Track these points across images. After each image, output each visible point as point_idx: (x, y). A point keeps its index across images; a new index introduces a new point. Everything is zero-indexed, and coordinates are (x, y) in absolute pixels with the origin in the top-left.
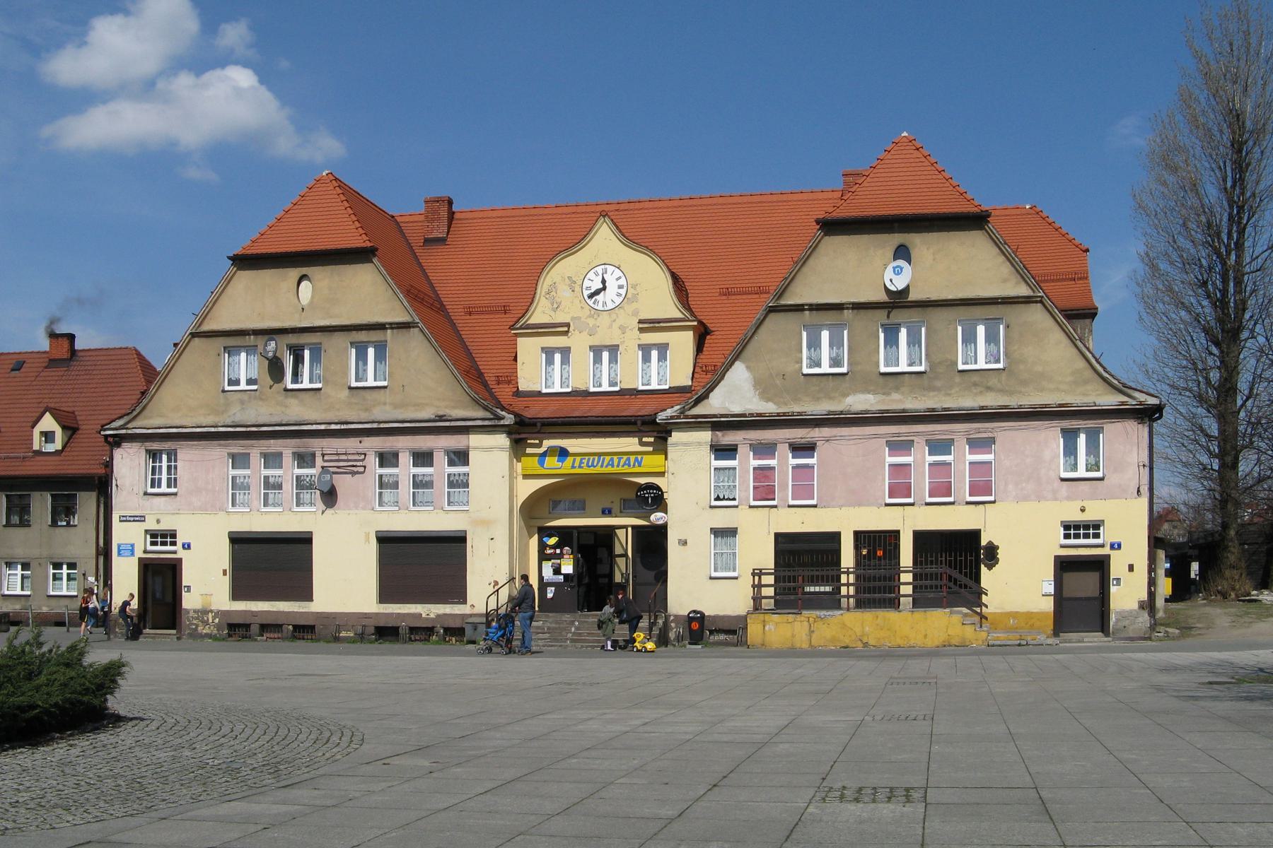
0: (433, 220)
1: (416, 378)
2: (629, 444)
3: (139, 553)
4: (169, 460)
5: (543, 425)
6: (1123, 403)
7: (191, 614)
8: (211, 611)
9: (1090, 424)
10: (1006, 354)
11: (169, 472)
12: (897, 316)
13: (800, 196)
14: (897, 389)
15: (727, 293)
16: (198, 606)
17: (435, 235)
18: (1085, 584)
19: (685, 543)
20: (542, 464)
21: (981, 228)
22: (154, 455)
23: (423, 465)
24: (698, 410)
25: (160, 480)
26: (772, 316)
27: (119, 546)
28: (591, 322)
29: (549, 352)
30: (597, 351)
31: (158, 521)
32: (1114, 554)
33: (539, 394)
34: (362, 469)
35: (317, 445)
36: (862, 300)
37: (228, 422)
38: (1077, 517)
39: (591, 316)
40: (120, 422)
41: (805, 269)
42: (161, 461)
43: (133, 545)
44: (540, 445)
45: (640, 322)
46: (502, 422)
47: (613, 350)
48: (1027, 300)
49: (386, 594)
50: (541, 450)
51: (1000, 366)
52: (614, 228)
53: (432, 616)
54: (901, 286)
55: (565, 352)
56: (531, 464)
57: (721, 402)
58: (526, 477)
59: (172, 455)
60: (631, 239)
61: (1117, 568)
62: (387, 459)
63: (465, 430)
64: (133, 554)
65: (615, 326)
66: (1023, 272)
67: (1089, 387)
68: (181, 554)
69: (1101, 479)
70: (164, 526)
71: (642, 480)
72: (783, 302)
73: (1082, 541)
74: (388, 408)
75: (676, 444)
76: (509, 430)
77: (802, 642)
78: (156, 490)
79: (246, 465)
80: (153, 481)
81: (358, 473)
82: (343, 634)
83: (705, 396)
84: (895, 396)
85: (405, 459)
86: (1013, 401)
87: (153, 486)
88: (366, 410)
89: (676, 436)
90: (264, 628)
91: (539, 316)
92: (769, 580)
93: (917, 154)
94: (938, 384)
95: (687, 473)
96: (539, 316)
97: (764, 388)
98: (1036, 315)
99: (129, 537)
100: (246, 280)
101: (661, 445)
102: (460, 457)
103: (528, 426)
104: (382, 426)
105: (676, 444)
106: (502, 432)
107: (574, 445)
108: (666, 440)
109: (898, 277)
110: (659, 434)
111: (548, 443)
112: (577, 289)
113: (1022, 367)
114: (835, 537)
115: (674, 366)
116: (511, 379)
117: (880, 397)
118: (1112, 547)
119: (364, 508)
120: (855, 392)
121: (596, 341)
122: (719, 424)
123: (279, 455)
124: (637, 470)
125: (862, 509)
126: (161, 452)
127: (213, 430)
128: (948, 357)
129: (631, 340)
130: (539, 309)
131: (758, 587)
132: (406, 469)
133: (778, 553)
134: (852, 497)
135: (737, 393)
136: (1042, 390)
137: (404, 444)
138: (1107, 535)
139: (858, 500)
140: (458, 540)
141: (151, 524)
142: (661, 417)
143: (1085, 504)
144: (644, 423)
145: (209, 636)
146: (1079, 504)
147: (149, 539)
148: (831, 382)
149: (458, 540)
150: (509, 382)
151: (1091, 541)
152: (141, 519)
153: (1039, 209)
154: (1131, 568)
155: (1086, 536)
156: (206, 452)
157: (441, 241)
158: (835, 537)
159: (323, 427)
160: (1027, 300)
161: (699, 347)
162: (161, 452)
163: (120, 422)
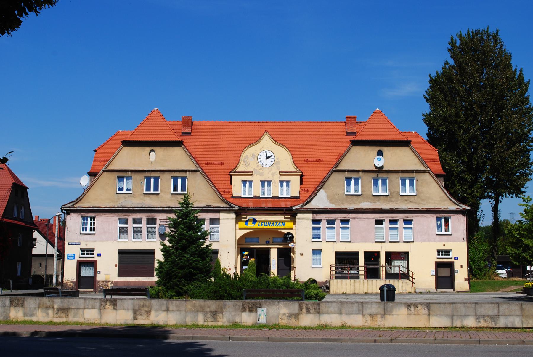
0: (185, 125)
2: (281, 218)
3: (77, 258)
4: (91, 220)
6: (457, 209)
7: (101, 282)
9: (446, 215)
10: (417, 190)
11: (91, 225)
12: (381, 175)
13: (329, 124)
14: (378, 201)
15: (307, 161)
16: (104, 280)
17: (186, 131)
18: (445, 272)
22: (84, 218)
24: (307, 206)
25: (86, 228)
26: (334, 173)
27: (68, 255)
28: (261, 171)
29: (244, 182)
30: (263, 182)
31: (86, 245)
32: (456, 261)
33: (241, 197)
35: (157, 216)
37: (119, 205)
38: (442, 248)
40: (71, 204)
41: (345, 157)
42: (87, 220)
43: (74, 255)
44: (246, 218)
45: (280, 172)
46: (234, 209)
47: (269, 182)
48: (424, 172)
50: (246, 220)
51: (415, 194)
52: (270, 137)
54: (380, 165)
55: (251, 182)
56: (242, 225)
57: (315, 204)
58: (240, 229)
60: (276, 141)
61: (457, 266)
63: (218, 212)
64: (74, 258)
65: (270, 173)
67: (446, 202)
68: (96, 258)
69: (451, 235)
70: (89, 247)
71: (286, 231)
72: (338, 169)
73: (444, 256)
75: (299, 219)
76: (236, 212)
78: (85, 232)
80: (83, 228)
83: (310, 201)
84: (378, 203)
86: (420, 207)
87: (83, 230)
89: (299, 216)
91: (240, 168)
92: (334, 268)
93: (382, 117)
94: (393, 199)
95: (302, 228)
96: (240, 168)
97: (331, 199)
98: (427, 176)
99: (72, 252)
100: (127, 151)
101: (293, 219)
105: (299, 219)
107: (258, 218)
108: (295, 217)
109: (379, 162)
110: (291, 214)
111: (249, 217)
112: (256, 159)
113: (422, 195)
114: (357, 253)
115: (294, 189)
116: (229, 191)
117: (373, 204)
118: (455, 258)
120: (364, 201)
121: (263, 178)
124: (283, 227)
126: (87, 217)
127: (113, 209)
128: (397, 190)
129: (277, 178)
130: (241, 166)
131: (331, 271)
133: (337, 259)
134: (363, 238)
135: (321, 201)
136: (429, 203)
138: (453, 255)
141: (83, 246)
142: (294, 208)
144: (286, 210)
146: (443, 243)
147: (81, 252)
148: (355, 198)
150: (228, 192)
151: (447, 256)
152: (79, 244)
153: (418, 133)
154: (462, 266)
155: (445, 255)
156: (109, 217)
157: (189, 133)
158: (357, 253)
159: (161, 209)
160: (424, 172)
161: (301, 183)
162: (87, 217)
163: (71, 204)
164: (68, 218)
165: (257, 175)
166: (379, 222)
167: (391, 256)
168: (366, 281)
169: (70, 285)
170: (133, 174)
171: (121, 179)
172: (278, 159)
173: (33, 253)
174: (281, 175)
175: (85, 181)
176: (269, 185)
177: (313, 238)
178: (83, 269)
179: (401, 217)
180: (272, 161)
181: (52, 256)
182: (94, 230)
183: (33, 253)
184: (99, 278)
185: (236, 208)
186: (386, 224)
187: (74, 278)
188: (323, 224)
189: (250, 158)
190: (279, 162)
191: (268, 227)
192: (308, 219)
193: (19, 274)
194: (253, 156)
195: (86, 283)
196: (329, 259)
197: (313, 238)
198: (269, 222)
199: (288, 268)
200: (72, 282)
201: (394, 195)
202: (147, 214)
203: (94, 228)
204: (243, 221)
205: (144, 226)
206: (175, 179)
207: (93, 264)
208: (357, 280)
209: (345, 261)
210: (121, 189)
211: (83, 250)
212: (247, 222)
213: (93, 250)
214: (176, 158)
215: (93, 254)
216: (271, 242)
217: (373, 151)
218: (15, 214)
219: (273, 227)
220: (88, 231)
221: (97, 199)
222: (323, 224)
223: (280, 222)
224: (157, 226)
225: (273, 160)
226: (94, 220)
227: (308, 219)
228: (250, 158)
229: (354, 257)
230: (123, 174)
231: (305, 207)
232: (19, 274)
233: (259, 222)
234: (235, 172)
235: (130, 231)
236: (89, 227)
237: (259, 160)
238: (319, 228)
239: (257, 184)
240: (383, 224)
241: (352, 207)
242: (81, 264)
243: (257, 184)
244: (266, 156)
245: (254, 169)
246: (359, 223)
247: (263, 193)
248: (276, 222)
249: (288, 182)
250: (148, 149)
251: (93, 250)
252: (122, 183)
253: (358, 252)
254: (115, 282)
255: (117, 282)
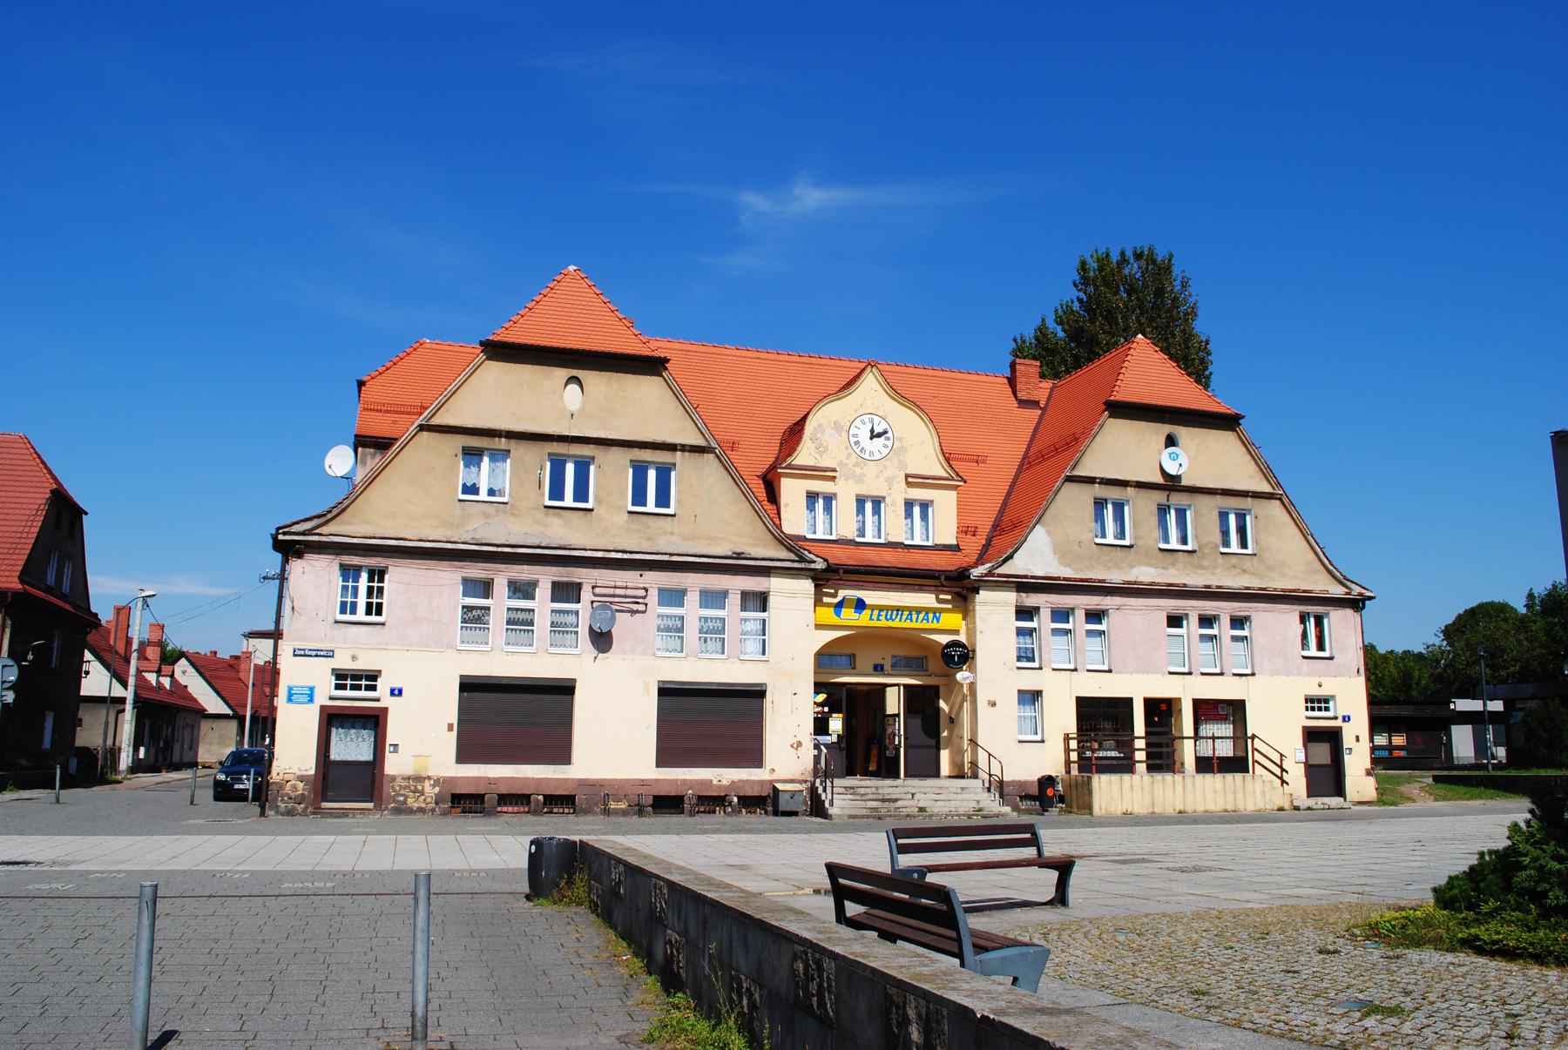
1: (706, 510)
2: (927, 599)
3: (322, 699)
4: (371, 579)
5: (846, 572)
7: (399, 782)
8: (429, 778)
10: (1196, 536)
14: (1173, 564)
16: (410, 772)
19: (994, 704)
20: (838, 614)
21: (1233, 430)
22: (349, 572)
23: (669, 605)
24: (1002, 570)
25: (354, 605)
27: (290, 689)
28: (858, 471)
29: (812, 497)
30: (861, 501)
31: (354, 658)
34: (641, 608)
36: (1142, 480)
37: (467, 537)
38: (1316, 692)
39: (857, 465)
40: (308, 525)
42: (356, 579)
43: (312, 689)
44: (834, 595)
45: (907, 476)
47: (877, 502)
49: (663, 759)
50: (836, 600)
53: (724, 782)
55: (829, 499)
59: (378, 574)
60: (899, 395)
62: (674, 597)
63: (765, 572)
64: (311, 701)
65: (882, 478)
66: (1267, 472)
68: (386, 701)
70: (363, 664)
72: (1076, 473)
74: (675, 539)
77: (1140, 807)
78: (348, 617)
79: (530, 596)
80: (344, 604)
81: (638, 612)
82: (613, 805)
84: (1172, 571)
85: (692, 599)
87: (343, 611)
88: (650, 539)
89: (984, 595)
90: (506, 799)
92: (1073, 744)
94: (1205, 563)
97: (1061, 552)
100: (496, 371)
102: (760, 601)
103: (833, 574)
104: (675, 558)
106: (807, 577)
107: (872, 597)
110: (960, 588)
111: (842, 593)
112: (845, 434)
114: (1128, 703)
117: (1160, 571)
119: (644, 653)
120: (1140, 564)
121: (863, 491)
122: (1025, 585)
123: (534, 584)
125: (1151, 676)
126: (357, 570)
127: (449, 546)
129: (897, 495)
131: (1068, 751)
132: (692, 610)
134: (1142, 663)
137: (694, 582)
139: (1145, 668)
140: (756, 694)
141: (343, 662)
143: (1322, 680)
145: (421, 810)
146: (1317, 680)
148: (1120, 553)
149: (756, 694)
151: (1323, 714)
152: (330, 654)
154: (1358, 739)
155: (1320, 709)
159: (600, 554)
162: (357, 570)
163: (308, 525)
164: (297, 567)
165: (846, 479)
166: (1175, 621)
167: (1206, 710)
168: (1200, 776)
169: (294, 787)
170: (513, 445)
171: (472, 456)
172: (900, 440)
173: (83, 693)
174: (909, 484)
175: (340, 460)
176: (877, 511)
177: (1019, 659)
178: (337, 735)
179: (1224, 609)
180: (886, 446)
181: (122, 700)
182: (379, 613)
183: (83, 693)
184: (394, 765)
185: (820, 565)
186: (1192, 627)
187: (309, 766)
188: (1044, 622)
189: (829, 431)
190: (903, 450)
191: (896, 624)
192: (1006, 604)
193: (47, 744)
194: (837, 426)
195: (349, 785)
196: (1061, 718)
197: (1019, 659)
198: (898, 609)
199: (933, 742)
200: (301, 778)
201: (1207, 551)
202: (554, 569)
203: (380, 606)
204: (828, 605)
205: (542, 604)
206: (640, 471)
207: (374, 721)
208: (1126, 777)
209: (1101, 719)
210: (472, 489)
211: (341, 676)
212: (840, 605)
213: (373, 676)
214: (640, 409)
215: (374, 688)
216: (888, 667)
217: (1155, 433)
218: (51, 578)
219: (908, 625)
220: (361, 615)
221: (388, 512)
222: (1044, 622)
223: (927, 610)
224: (583, 607)
225: (889, 443)
226: (381, 580)
227: (1006, 604)
228: (829, 431)
229: (1386, 711)
230: (480, 442)
231: (999, 571)
232: (47, 744)
233: (873, 608)
234: (789, 467)
235: (497, 619)
236: (362, 600)
237: (853, 440)
238: (1030, 632)
239: (845, 507)
240: (1180, 626)
241: (1115, 577)
242: (332, 719)
243: (845, 507)
244: (872, 431)
245: (840, 463)
246: (1136, 621)
247: (862, 533)
248: (919, 610)
249: (925, 506)
250: (562, 374)
251: (373, 676)
252: (474, 469)
253: (1131, 700)
254: (446, 780)
255: (453, 780)
